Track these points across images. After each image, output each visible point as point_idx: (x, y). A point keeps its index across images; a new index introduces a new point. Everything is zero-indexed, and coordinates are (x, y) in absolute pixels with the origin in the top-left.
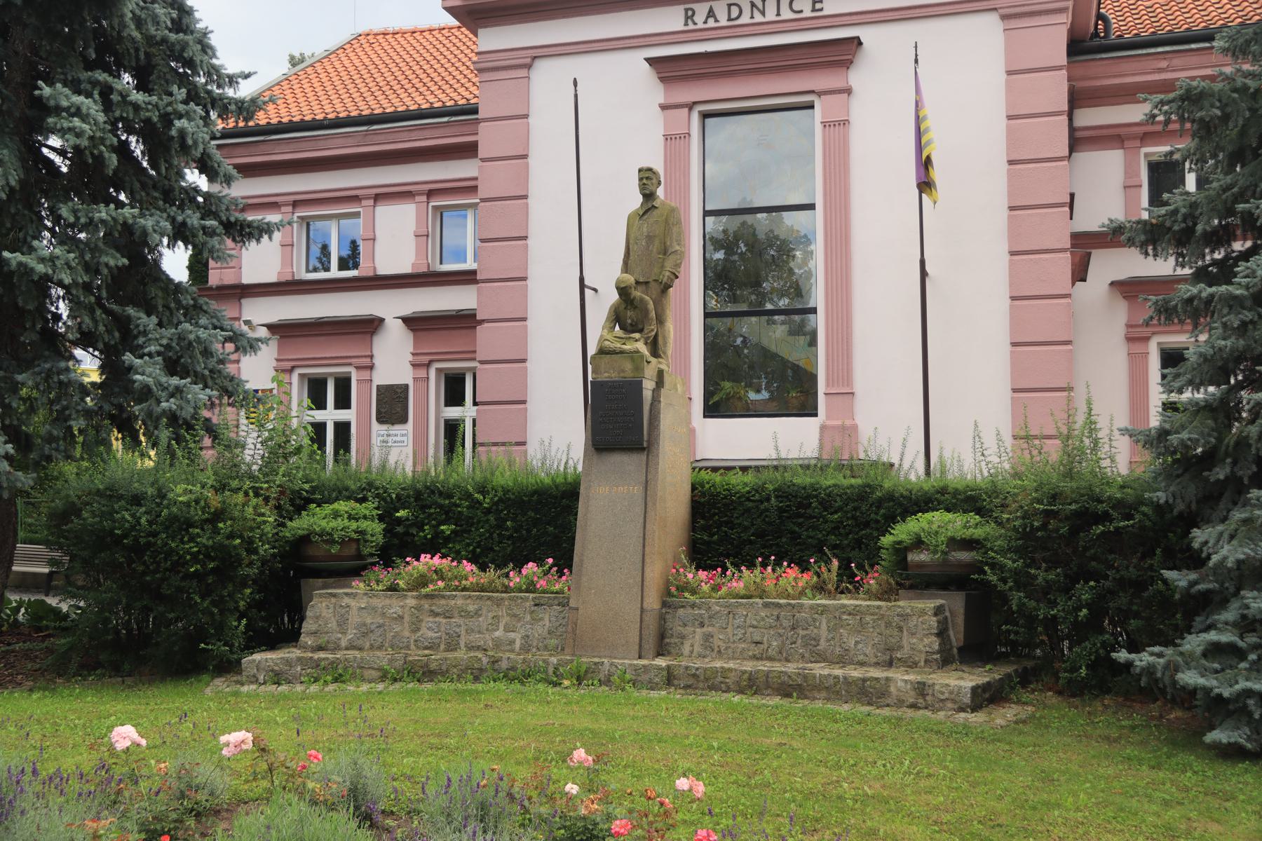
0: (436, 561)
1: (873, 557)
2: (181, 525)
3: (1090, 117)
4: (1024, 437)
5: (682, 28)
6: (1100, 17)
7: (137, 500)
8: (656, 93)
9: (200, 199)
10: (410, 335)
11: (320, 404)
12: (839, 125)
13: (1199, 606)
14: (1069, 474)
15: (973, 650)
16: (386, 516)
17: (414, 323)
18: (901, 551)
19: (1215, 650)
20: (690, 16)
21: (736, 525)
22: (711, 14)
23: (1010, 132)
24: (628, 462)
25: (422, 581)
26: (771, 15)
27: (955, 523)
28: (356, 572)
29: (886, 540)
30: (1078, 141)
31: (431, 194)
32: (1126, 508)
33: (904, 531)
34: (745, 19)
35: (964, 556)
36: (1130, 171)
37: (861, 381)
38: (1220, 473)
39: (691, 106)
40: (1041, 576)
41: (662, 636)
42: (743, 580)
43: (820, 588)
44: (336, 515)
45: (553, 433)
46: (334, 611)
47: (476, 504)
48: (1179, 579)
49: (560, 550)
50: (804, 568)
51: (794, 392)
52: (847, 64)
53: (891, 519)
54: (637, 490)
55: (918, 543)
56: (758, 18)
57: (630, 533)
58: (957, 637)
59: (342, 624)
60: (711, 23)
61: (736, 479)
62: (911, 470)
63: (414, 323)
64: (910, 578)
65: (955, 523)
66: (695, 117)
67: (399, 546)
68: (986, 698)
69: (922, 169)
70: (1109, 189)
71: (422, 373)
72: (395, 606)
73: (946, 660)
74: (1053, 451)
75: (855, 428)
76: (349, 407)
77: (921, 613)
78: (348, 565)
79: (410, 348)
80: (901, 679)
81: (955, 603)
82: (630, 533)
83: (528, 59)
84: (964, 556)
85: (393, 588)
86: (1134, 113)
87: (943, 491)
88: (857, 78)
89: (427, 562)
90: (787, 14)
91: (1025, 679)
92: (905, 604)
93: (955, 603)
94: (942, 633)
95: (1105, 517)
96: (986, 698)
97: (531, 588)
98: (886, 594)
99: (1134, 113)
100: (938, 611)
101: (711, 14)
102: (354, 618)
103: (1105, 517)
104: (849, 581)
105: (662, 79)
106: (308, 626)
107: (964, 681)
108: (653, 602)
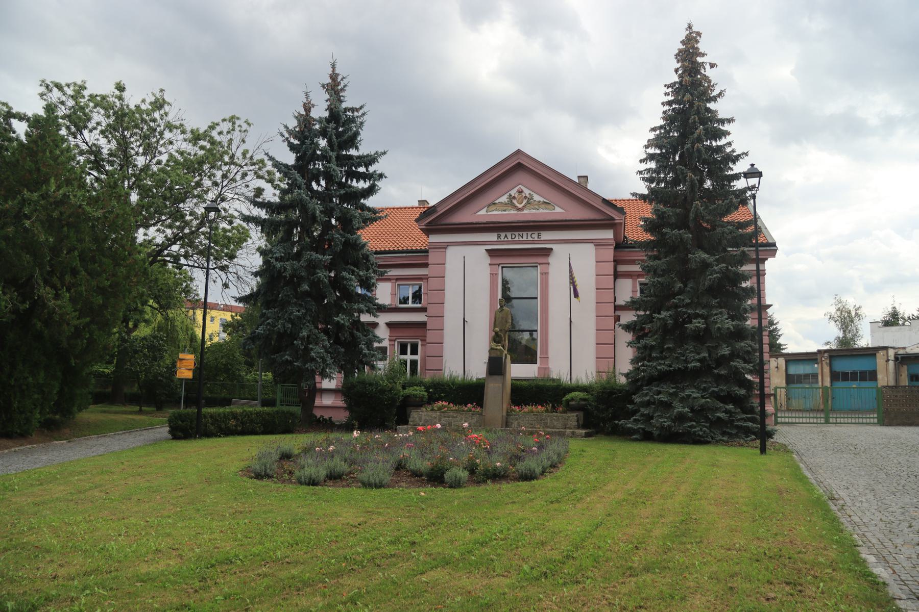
0: (444, 403)
1: (560, 403)
2: (383, 391)
3: (622, 268)
4: (598, 372)
6: (625, 237)
7: (371, 384)
8: (488, 260)
10: (388, 330)
11: (414, 363)
12: (545, 275)
13: (634, 412)
14: (608, 383)
15: (584, 426)
16: (427, 391)
17: (390, 325)
18: (568, 401)
19: (635, 420)
20: (499, 237)
21: (524, 394)
22: (506, 236)
23: (597, 279)
24: (499, 378)
25: (440, 409)
26: (525, 238)
27: (581, 395)
28: (421, 406)
29: (564, 399)
30: (617, 275)
31: (397, 280)
32: (620, 391)
33: (569, 396)
34: (517, 239)
35: (583, 403)
36: (634, 286)
37: (551, 354)
38: (639, 384)
40: (601, 407)
41: (507, 423)
42: (527, 409)
43: (547, 411)
45: (478, 370)
46: (415, 415)
47: (451, 388)
48: (630, 407)
49: (480, 402)
50: (542, 406)
51: (527, 355)
52: (548, 255)
53: (564, 395)
54: (500, 385)
55: (572, 399)
57: (497, 397)
58: (581, 422)
59: (420, 419)
61: (524, 383)
62: (565, 378)
63: (390, 325)
64: (570, 408)
65: (581, 395)
67: (431, 400)
70: (627, 291)
71: (392, 343)
72: (434, 415)
73: (578, 428)
74: (604, 376)
77: (573, 417)
78: (419, 404)
79: (388, 334)
80: (568, 431)
81: (581, 414)
82: (497, 397)
83: (445, 246)
84: (583, 403)
85: (433, 410)
86: (636, 268)
87: (578, 387)
88: (551, 260)
89: (440, 403)
90: (530, 238)
91: (597, 433)
92: (569, 414)
93: (581, 414)
94: (578, 421)
95: (615, 393)
96: (588, 435)
97: (470, 411)
98: (565, 412)
99: (636, 268)
101: (506, 236)
102: (423, 418)
103: (615, 393)
104: (554, 409)
106: (410, 419)
108: (505, 414)
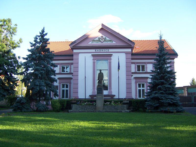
5: (95, 51)
8: (92, 58)
9: (33, 67)
20: (96, 51)
22: (98, 50)
34: (101, 51)
39: (96, 59)
44: (169, 101)
56: (103, 51)
60: (98, 51)
66: (96, 60)
68: (130, 112)
69: (147, 62)
75: (112, 92)
76: (139, 89)
88: (112, 58)
96: (130, 112)
100: (126, 106)
101: (98, 50)
105: (93, 57)
107: (128, 111)
